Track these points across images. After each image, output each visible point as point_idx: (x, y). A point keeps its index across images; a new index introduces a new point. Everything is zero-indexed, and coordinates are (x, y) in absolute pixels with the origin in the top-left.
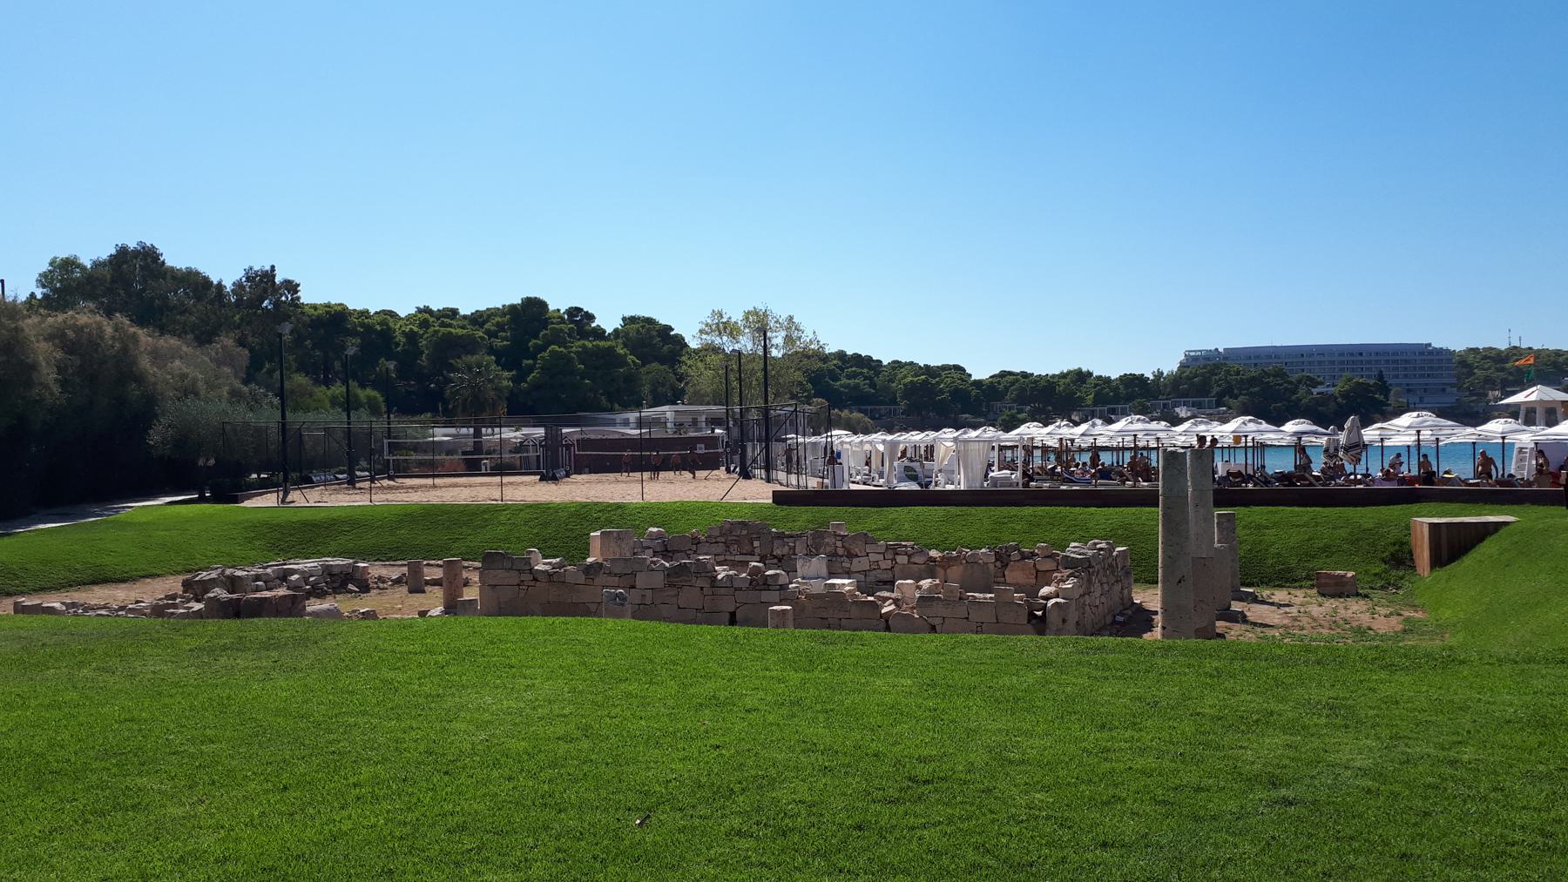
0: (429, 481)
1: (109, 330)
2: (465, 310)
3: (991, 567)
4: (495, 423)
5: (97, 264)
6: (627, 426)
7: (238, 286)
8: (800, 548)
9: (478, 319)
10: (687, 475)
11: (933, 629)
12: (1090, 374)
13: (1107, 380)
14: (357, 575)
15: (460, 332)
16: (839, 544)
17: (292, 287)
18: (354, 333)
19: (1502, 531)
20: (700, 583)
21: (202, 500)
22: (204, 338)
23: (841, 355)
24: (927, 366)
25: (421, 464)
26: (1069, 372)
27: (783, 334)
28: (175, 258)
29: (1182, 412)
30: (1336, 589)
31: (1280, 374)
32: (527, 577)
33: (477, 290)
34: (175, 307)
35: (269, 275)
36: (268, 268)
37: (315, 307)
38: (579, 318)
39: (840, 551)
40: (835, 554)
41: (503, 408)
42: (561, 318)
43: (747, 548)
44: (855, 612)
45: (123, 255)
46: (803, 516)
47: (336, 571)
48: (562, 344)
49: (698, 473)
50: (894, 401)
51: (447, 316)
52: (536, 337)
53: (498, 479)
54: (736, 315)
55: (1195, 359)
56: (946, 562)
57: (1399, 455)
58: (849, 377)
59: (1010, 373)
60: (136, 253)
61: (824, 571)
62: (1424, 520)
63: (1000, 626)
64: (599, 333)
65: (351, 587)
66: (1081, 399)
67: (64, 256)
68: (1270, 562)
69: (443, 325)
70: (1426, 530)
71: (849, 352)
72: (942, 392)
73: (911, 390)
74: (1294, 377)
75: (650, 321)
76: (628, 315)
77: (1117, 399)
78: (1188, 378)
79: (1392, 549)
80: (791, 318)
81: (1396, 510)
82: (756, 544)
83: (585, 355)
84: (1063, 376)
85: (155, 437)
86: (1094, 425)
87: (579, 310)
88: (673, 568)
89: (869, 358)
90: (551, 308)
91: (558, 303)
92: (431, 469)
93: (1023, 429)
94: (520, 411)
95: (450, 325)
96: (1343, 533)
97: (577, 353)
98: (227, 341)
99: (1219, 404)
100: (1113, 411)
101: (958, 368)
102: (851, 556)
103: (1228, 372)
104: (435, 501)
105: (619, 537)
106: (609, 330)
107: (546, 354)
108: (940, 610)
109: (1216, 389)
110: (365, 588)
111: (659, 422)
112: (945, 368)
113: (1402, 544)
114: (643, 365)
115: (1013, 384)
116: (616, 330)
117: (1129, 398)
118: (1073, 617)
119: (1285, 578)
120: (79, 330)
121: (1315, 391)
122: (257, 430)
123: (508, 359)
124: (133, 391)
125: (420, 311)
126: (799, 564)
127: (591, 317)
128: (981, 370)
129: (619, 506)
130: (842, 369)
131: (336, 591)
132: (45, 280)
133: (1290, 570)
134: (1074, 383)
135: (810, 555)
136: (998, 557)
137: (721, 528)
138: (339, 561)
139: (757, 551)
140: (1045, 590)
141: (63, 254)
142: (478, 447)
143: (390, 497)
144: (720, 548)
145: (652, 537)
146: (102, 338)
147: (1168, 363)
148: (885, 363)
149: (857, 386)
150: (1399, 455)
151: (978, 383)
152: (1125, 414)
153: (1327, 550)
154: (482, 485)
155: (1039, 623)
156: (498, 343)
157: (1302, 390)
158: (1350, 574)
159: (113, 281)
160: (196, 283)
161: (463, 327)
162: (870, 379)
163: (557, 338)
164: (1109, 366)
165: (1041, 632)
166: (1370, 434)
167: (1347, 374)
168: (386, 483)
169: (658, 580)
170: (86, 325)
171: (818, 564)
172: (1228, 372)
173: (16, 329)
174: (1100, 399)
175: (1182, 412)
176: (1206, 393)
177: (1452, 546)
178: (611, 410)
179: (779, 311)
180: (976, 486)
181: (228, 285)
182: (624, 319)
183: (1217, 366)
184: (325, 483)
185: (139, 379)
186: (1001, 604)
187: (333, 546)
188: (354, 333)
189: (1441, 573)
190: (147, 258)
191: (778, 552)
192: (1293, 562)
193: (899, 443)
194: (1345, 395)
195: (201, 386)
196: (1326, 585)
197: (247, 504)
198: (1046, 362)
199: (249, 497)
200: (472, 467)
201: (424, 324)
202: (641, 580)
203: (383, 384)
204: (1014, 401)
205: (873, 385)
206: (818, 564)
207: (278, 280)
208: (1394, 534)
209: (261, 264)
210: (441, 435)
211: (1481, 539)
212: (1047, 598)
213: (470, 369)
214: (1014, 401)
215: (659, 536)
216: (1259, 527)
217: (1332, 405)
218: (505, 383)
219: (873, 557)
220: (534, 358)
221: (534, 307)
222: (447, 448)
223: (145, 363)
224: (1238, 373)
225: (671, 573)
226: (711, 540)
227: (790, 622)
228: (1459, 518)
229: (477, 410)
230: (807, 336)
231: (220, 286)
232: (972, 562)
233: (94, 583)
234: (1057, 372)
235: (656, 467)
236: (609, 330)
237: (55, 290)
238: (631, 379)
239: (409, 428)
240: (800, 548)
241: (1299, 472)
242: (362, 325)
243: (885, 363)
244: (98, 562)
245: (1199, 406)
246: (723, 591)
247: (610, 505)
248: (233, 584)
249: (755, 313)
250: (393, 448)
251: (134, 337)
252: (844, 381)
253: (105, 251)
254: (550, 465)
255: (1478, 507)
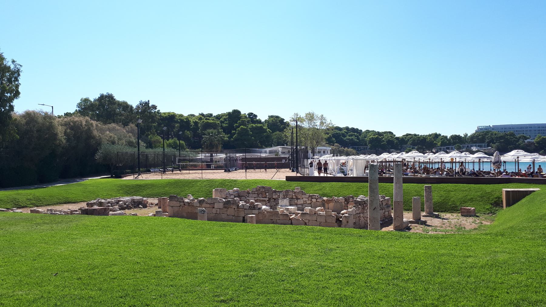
0: (188, 171)
1: (84, 123)
2: (215, 114)
3: (343, 203)
4: (217, 152)
5: (95, 100)
6: (265, 153)
7: (138, 107)
8: (281, 196)
9: (218, 117)
10: (263, 170)
11: (306, 224)
12: (440, 135)
13: (446, 137)
14: (143, 202)
15: (211, 121)
16: (294, 195)
17: (154, 107)
18: (177, 122)
19: (531, 196)
20: (234, 207)
21: (112, 177)
22: (125, 124)
23: (347, 128)
24: (378, 132)
25: (192, 166)
26: (432, 134)
27: (320, 121)
28: (119, 97)
29: (474, 149)
30: (467, 214)
31: (512, 135)
32: (182, 204)
33: (219, 107)
34: (118, 114)
35: (147, 104)
36: (147, 101)
37: (165, 114)
38: (252, 117)
39: (294, 197)
40: (292, 198)
41: (220, 148)
42: (246, 117)
43: (264, 196)
44: (281, 217)
45: (102, 97)
46: (295, 186)
47: (135, 201)
48: (245, 125)
49: (267, 170)
50: (366, 145)
51: (208, 116)
52: (237, 123)
53: (201, 171)
54: (303, 115)
55: (481, 129)
56: (328, 201)
57: (530, 165)
58: (349, 136)
59: (410, 135)
60: (106, 96)
61: (288, 204)
62: (506, 188)
63: (327, 224)
64: (259, 122)
65: (140, 206)
66: (436, 144)
67: (85, 97)
68: (450, 204)
69: (206, 119)
70: (504, 194)
71: (350, 127)
72: (383, 141)
73: (372, 141)
74: (518, 136)
75: (277, 117)
76: (270, 115)
77: (450, 144)
78: (477, 136)
79: (495, 200)
80: (322, 115)
81: (496, 186)
82: (267, 194)
83: (253, 129)
84: (430, 135)
85: (97, 157)
86: (402, 154)
87: (252, 114)
88: (226, 202)
89: (357, 129)
90: (242, 113)
91: (244, 111)
92: (194, 168)
93: (382, 155)
94: (227, 147)
95: (209, 119)
96: (479, 194)
97: (250, 128)
98: (132, 126)
99: (488, 146)
100: (448, 148)
101: (390, 133)
102: (297, 199)
103: (492, 134)
104: (186, 178)
105: (221, 191)
106: (263, 120)
107: (239, 129)
108: (308, 217)
109: (487, 141)
110: (145, 206)
111: (276, 152)
112: (385, 133)
113: (499, 198)
114: (273, 132)
115: (411, 138)
116: (266, 120)
117: (454, 144)
118: (352, 221)
119: (453, 209)
120: (75, 122)
121: (526, 141)
122: (131, 154)
123: (227, 130)
124: (93, 142)
125: (200, 114)
126: (280, 201)
127: (256, 116)
128: (399, 133)
129: (235, 181)
130: (347, 133)
131: (135, 207)
132: (79, 105)
133: (456, 207)
134: (434, 138)
135: (284, 198)
136: (346, 200)
137: (256, 189)
138: (138, 198)
139: (268, 196)
140: (342, 212)
141: (84, 97)
142: (212, 160)
143: (430, 156)
144: (256, 195)
145: (234, 191)
146: (81, 125)
147: (470, 131)
148: (363, 131)
149: (352, 139)
150: (530, 165)
151: (398, 138)
152: (453, 149)
153: (471, 200)
154: (210, 173)
155: (339, 222)
156: (224, 125)
157: (520, 141)
158: (472, 209)
159: (99, 106)
160: (125, 106)
161: (213, 120)
162: (357, 136)
163: (243, 123)
164: (448, 132)
165: (340, 226)
166: (503, 158)
167: (540, 135)
168: (179, 172)
169: (221, 205)
170: (77, 121)
171: (286, 201)
172: (492, 134)
173: (51, 122)
174: (443, 144)
175: (474, 149)
176: (483, 142)
177: (514, 198)
178: (262, 148)
179: (318, 113)
180: (361, 175)
181: (134, 106)
182: (269, 116)
183: (488, 132)
184: (155, 172)
185: (94, 137)
186: (328, 216)
187: (145, 193)
188: (177, 122)
189: (508, 208)
190: (110, 97)
191: (274, 197)
192: (458, 204)
193: (339, 160)
194: (538, 143)
195: (116, 139)
196: (464, 212)
197: (124, 178)
198: (423, 131)
199: (126, 177)
200: (208, 167)
201: (200, 119)
202: (216, 206)
203: (186, 139)
204: (411, 144)
205: (358, 139)
206: (286, 201)
207: (150, 105)
208: (497, 194)
209: (145, 100)
210: (201, 156)
211: (524, 197)
212: (343, 214)
213: (209, 134)
214: (411, 144)
215: (237, 191)
216: (449, 191)
217: (533, 146)
218: (226, 139)
219: (305, 199)
220: (236, 130)
221: (236, 113)
222: (201, 160)
223: (96, 133)
224: (496, 134)
225: (225, 203)
226: (253, 193)
227: (255, 221)
228: (512, 190)
229: (211, 148)
230: (328, 121)
231: (132, 107)
232: (337, 202)
233: (65, 203)
234: (428, 134)
235: (266, 167)
236: (263, 120)
237: (82, 109)
238: (268, 137)
239: (188, 153)
240: (281, 196)
241: (491, 172)
242: (180, 119)
243: (363, 131)
244: (68, 196)
245: (481, 146)
246: (241, 210)
247: (233, 180)
248: (101, 204)
249: (310, 114)
250: (180, 161)
251: (92, 124)
252: (348, 137)
253: (97, 96)
254: (228, 166)
255: (507, 185)
